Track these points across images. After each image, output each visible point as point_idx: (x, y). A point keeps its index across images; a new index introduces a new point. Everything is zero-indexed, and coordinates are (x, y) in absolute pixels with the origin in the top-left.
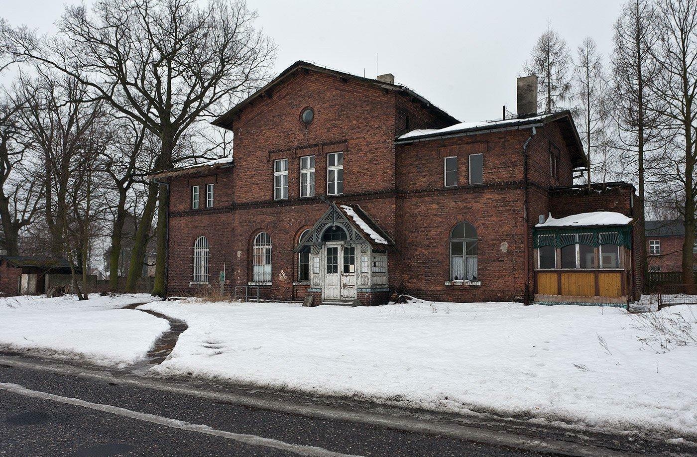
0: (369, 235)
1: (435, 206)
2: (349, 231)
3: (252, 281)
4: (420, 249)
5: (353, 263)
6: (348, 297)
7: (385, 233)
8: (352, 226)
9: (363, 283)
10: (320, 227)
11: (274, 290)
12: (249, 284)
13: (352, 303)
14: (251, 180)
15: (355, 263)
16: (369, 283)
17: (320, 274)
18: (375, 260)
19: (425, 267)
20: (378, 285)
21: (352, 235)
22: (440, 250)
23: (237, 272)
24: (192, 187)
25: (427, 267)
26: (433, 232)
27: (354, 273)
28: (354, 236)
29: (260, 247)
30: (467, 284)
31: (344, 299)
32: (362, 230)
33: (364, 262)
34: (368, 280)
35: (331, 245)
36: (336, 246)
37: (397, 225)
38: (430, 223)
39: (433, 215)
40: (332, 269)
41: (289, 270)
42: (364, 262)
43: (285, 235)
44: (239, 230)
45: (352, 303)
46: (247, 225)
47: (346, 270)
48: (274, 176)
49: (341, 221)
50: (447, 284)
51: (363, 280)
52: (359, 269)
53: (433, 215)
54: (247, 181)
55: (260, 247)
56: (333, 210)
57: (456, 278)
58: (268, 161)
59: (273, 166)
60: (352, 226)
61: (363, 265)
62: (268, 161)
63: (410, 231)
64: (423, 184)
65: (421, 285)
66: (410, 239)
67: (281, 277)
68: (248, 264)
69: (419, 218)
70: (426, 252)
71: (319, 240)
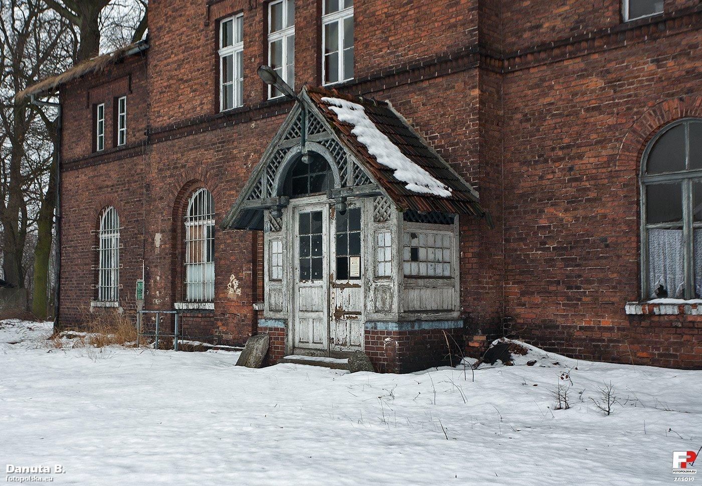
0: (393, 171)
1: (595, 82)
2: (338, 163)
3: (183, 299)
4: (552, 210)
5: (356, 252)
6: (344, 344)
7: (451, 170)
8: (346, 150)
9: (379, 305)
10: (276, 158)
11: (217, 320)
12: (177, 306)
13: (345, 361)
14: (177, 73)
15: (362, 250)
16: (395, 307)
17: (284, 282)
18: (415, 242)
19: (568, 262)
20: (426, 312)
21: (345, 174)
22: (609, 208)
23: (155, 281)
24: (95, 106)
25: (572, 259)
26: (589, 160)
27: (359, 278)
28: (350, 176)
29: (197, 223)
30: (694, 312)
31: (337, 348)
32: (374, 158)
33: (382, 244)
34: (392, 297)
35: (308, 205)
36: (318, 209)
37: (486, 146)
38: (579, 134)
39: (587, 110)
40: (311, 270)
41: (246, 273)
42: (382, 244)
43: (237, 191)
44: (159, 188)
45: (345, 361)
46: (171, 176)
47: (342, 271)
48: (217, 57)
49: (321, 137)
50: (630, 310)
51: (379, 299)
52: (371, 269)
53: (587, 110)
54: (171, 78)
55: (197, 223)
56: (303, 109)
57: (662, 293)
58: (207, 25)
59: (217, 33)
60: (346, 150)
61: (380, 257)
62: (207, 25)
63: (526, 163)
64: (559, 23)
65: (555, 312)
66: (525, 185)
67: (231, 291)
68: (173, 263)
69: (550, 121)
70: (568, 218)
71: (274, 194)
